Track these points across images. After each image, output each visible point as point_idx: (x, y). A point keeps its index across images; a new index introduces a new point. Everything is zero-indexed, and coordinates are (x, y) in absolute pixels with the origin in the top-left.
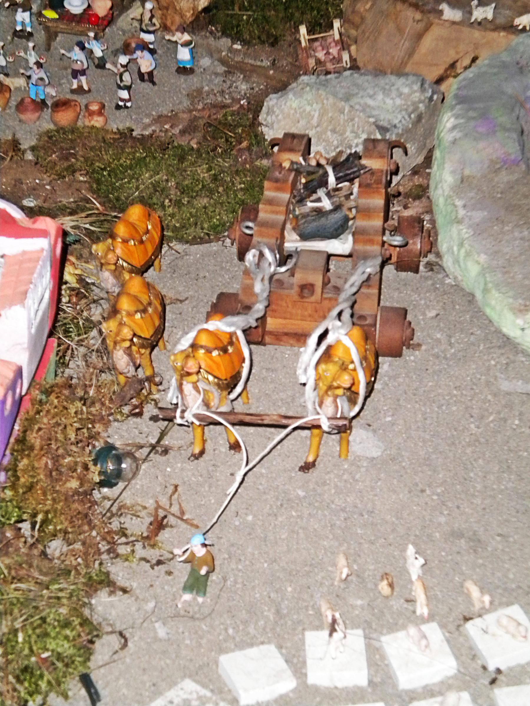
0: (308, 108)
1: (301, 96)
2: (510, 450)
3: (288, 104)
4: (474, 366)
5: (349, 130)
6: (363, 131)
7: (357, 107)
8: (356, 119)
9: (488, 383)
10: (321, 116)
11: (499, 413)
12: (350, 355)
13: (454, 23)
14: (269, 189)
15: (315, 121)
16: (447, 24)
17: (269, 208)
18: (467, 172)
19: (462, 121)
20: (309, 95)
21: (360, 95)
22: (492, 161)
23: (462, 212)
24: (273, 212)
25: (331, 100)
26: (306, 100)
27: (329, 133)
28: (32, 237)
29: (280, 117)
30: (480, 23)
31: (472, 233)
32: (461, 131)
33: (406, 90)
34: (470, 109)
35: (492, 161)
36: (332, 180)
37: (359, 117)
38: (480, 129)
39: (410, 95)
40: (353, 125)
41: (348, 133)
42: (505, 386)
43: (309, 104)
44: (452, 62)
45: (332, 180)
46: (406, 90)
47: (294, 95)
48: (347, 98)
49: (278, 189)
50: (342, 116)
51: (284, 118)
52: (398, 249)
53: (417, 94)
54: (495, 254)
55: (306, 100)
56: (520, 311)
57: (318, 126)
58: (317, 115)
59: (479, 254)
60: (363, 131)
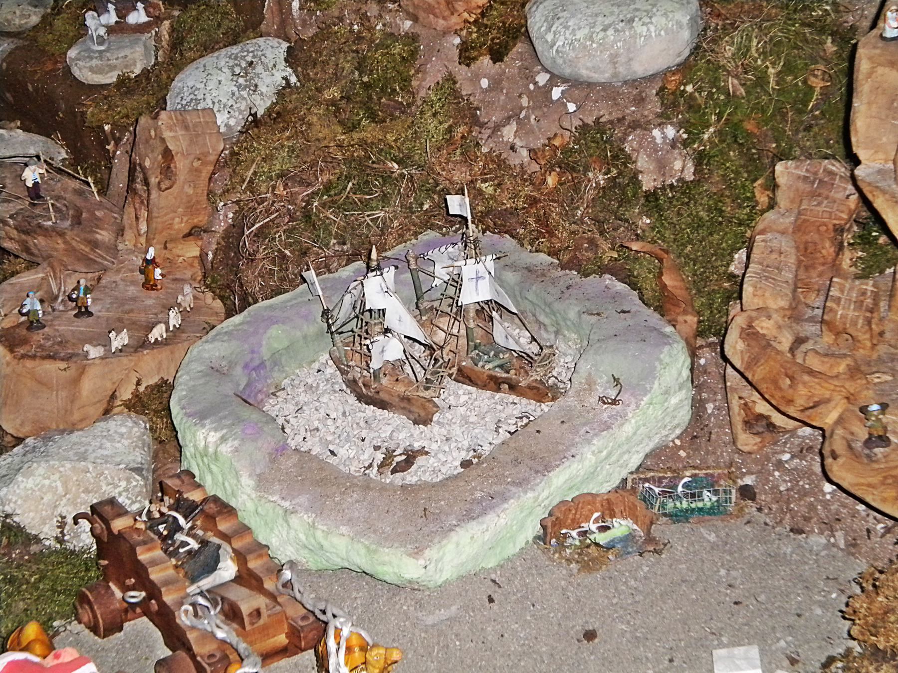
0: (47, 482)
1: (32, 475)
2: (469, 667)
3: (21, 487)
4: (393, 618)
5: (103, 484)
6: (120, 480)
7: (98, 461)
8: (106, 472)
9: (414, 625)
10: (65, 484)
11: (438, 643)
12: (363, 638)
13: (102, 358)
14: (142, 553)
15: (60, 490)
16: (97, 361)
17: (156, 568)
18: (258, 471)
19: (225, 431)
20: (40, 469)
21: (90, 451)
22: (269, 453)
23: (286, 504)
24: (161, 570)
25: (68, 465)
26: (40, 475)
27: (83, 495)
28: (80, 667)
29: (19, 502)
30: (121, 351)
31: (314, 515)
32: (235, 439)
33: (123, 430)
34: (221, 419)
35: (269, 453)
36: (182, 521)
37: (107, 469)
38: (248, 431)
39: (130, 432)
40: (106, 478)
41: (104, 488)
42: (430, 620)
43: (45, 478)
44: (111, 393)
45: (182, 521)
46: (123, 430)
47: (23, 476)
48: (83, 457)
49: (150, 550)
50: (88, 475)
51: (25, 501)
52: (819, 447)
53: (136, 429)
54: (350, 522)
55: (40, 475)
56: (417, 553)
57: (66, 494)
58: (59, 484)
59: (337, 527)
60: (120, 480)
